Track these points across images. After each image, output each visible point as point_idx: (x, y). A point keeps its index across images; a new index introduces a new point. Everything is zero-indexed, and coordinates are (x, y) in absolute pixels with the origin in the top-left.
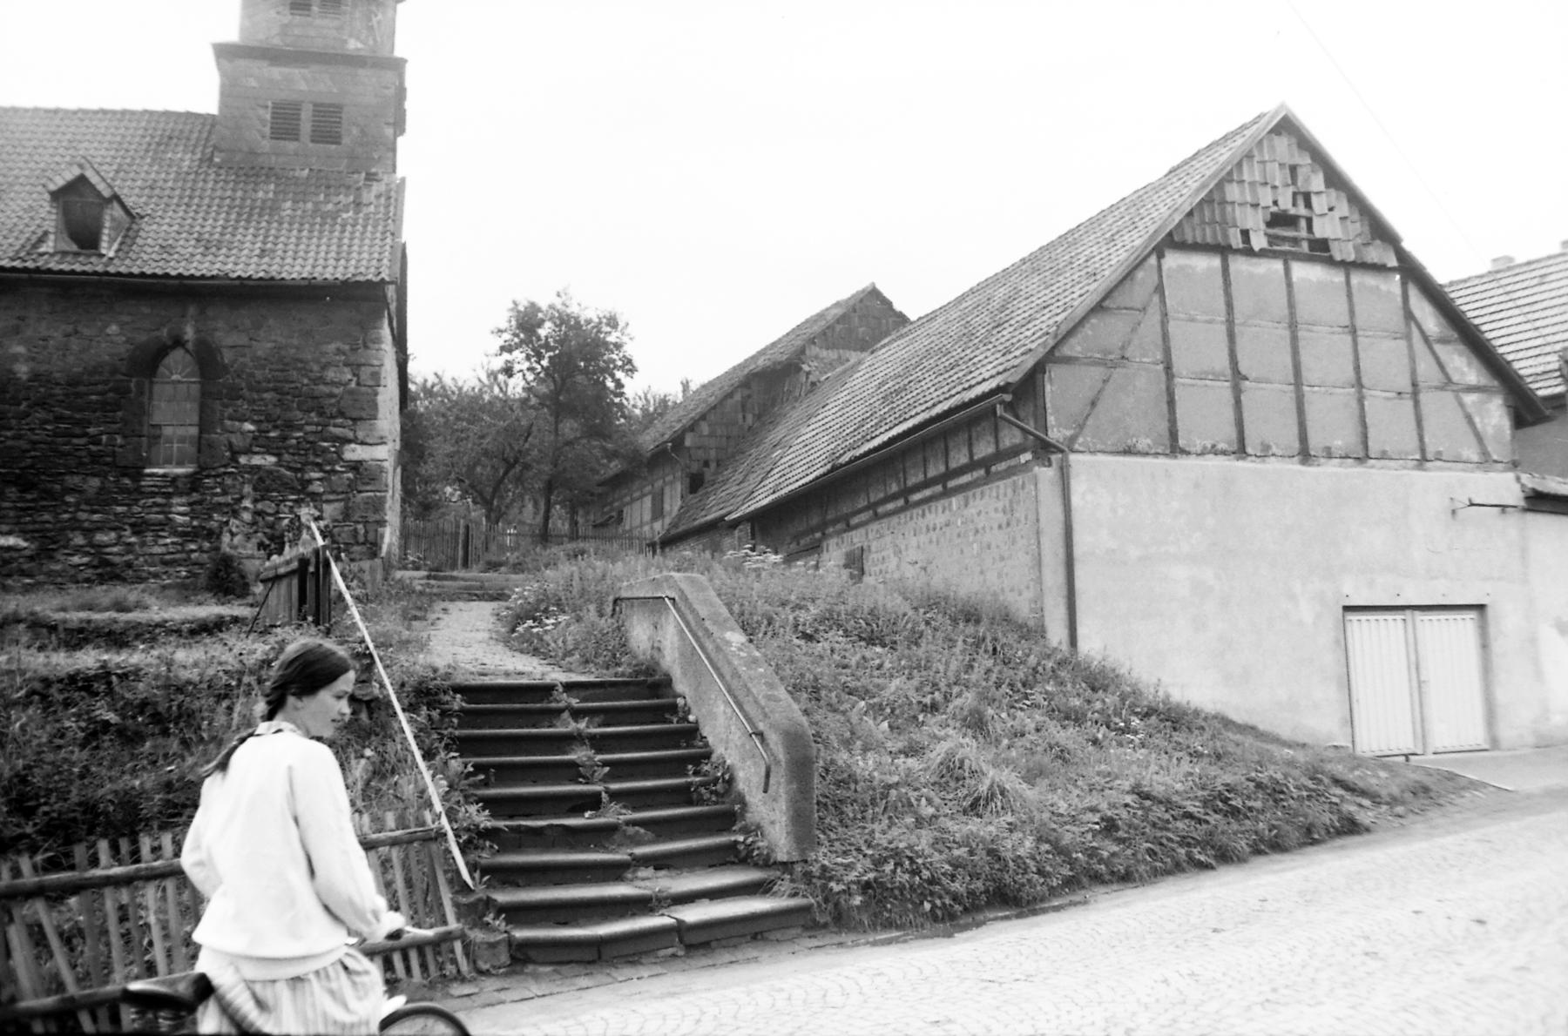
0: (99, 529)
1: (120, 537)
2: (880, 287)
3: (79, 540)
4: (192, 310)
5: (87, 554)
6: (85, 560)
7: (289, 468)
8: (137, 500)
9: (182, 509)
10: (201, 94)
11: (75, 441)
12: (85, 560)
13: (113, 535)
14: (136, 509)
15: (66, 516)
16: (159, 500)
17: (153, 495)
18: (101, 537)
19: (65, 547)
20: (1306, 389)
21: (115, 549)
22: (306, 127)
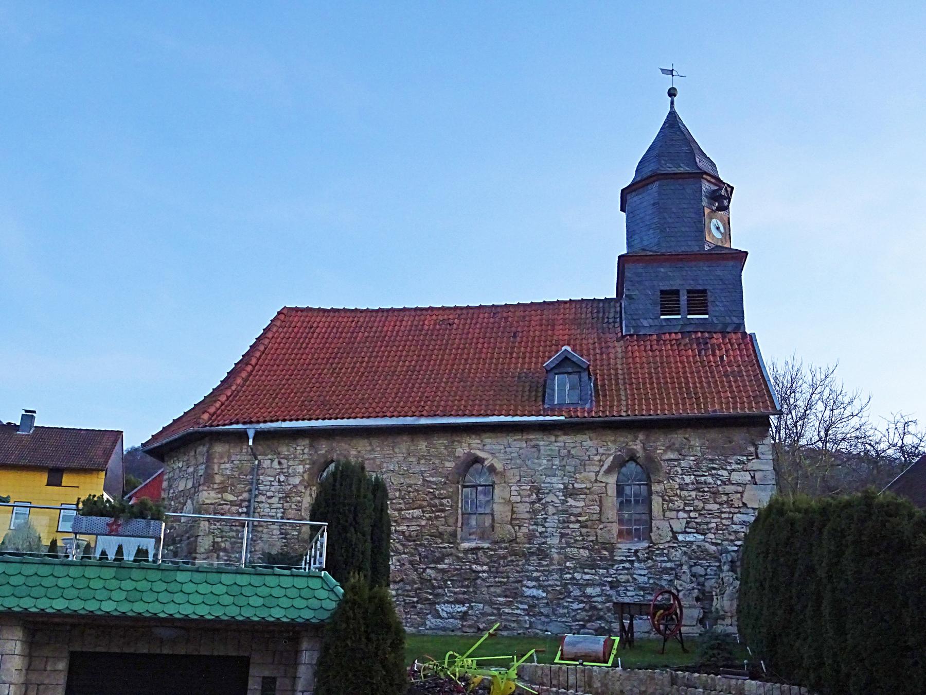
0: (588, 585)
1: (603, 590)
2: (619, 208)
3: (577, 593)
4: (641, 436)
5: (582, 602)
6: (581, 606)
7: (713, 544)
8: (612, 565)
9: (643, 572)
10: (605, 287)
11: (571, 526)
12: (581, 606)
13: (598, 589)
14: (612, 571)
15: (569, 576)
16: (627, 565)
17: (622, 562)
18: (589, 590)
19: (569, 596)
20: (202, 449)
21: (599, 599)
22: (684, 298)
